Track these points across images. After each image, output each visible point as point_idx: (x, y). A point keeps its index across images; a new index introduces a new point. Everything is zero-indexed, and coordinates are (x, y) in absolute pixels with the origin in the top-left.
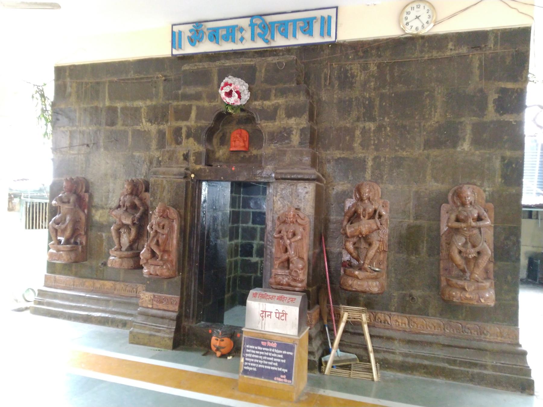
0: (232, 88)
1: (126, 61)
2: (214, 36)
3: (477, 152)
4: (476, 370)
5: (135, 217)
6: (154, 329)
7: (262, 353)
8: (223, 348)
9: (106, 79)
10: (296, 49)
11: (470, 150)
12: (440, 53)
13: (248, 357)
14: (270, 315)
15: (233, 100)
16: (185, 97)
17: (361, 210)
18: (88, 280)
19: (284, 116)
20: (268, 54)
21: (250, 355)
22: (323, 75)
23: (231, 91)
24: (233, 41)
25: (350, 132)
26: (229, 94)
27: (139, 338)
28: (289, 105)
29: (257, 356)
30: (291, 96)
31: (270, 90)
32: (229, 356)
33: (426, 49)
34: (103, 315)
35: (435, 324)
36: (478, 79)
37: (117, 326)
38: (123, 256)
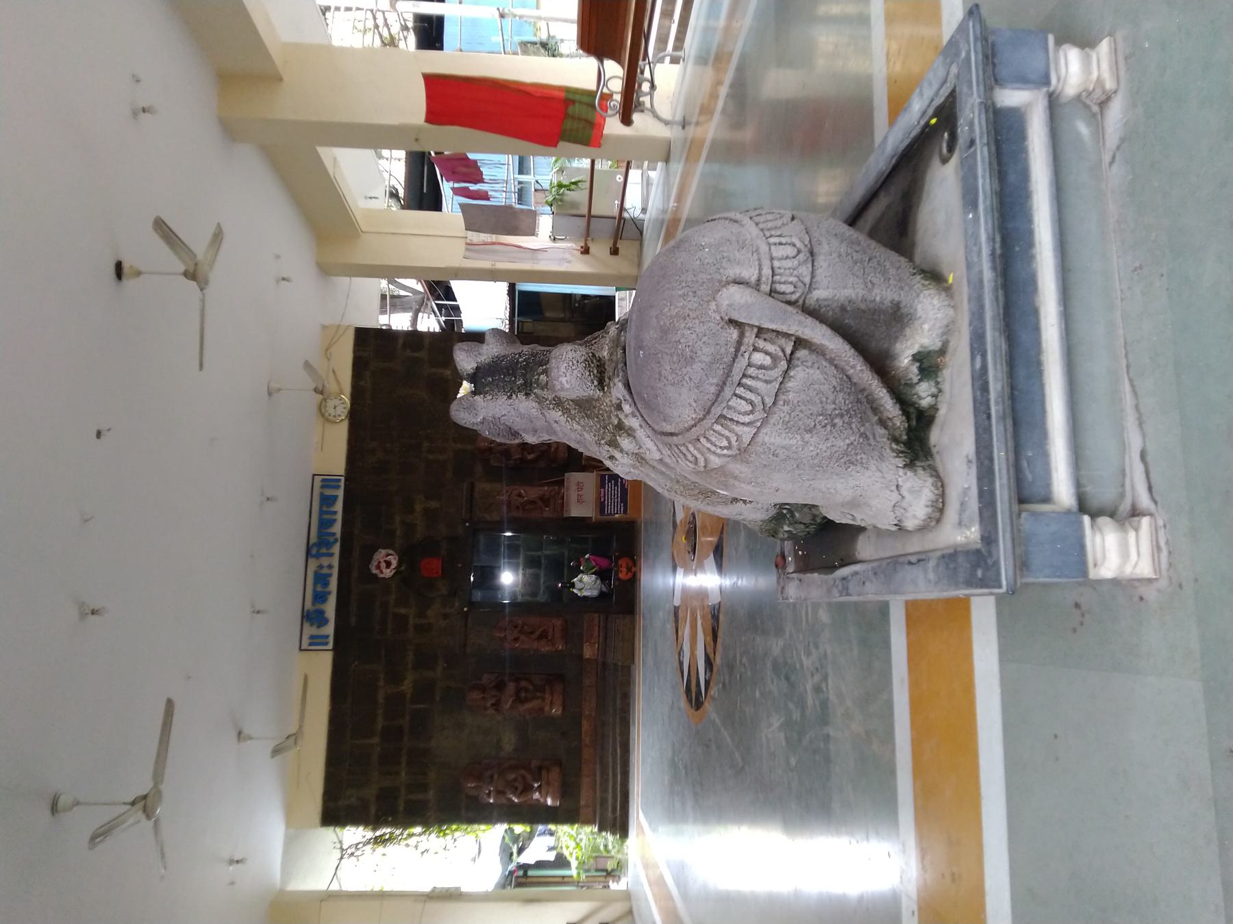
2: (320, 597)
15: (394, 563)
24: (330, 575)
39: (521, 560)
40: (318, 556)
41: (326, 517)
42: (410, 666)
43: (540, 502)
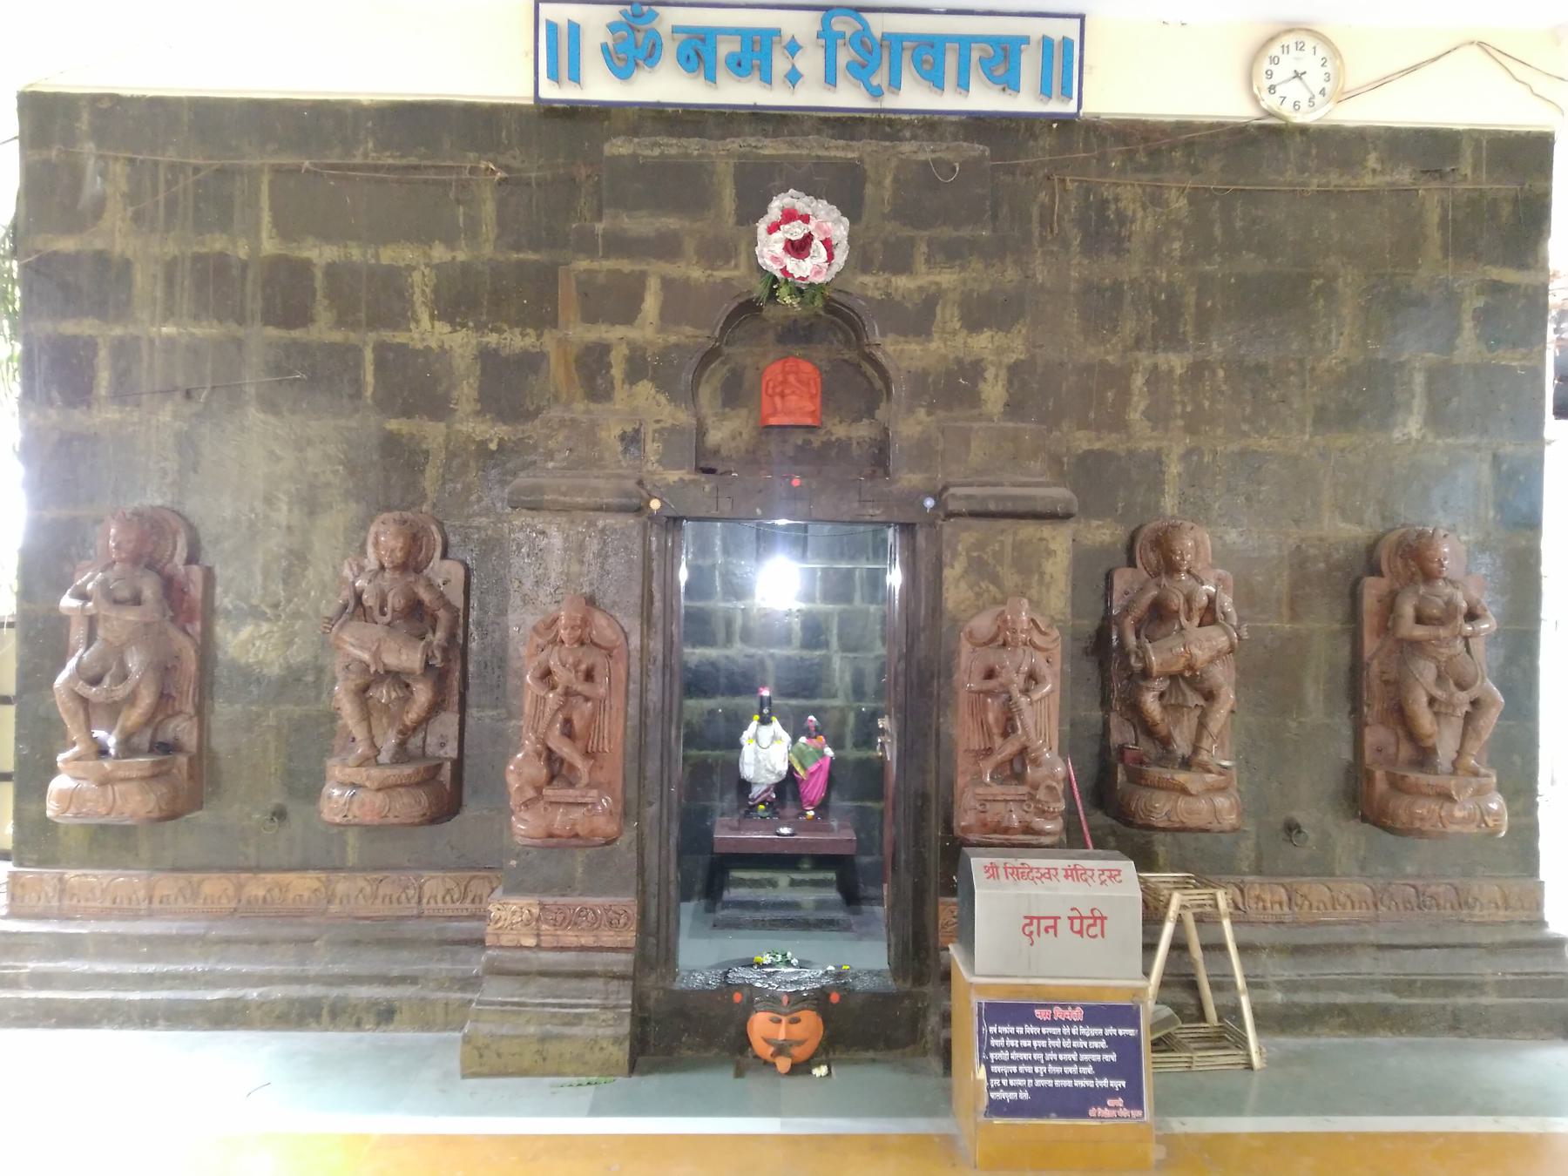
0: (811, 227)
1: (344, 103)
3: (1439, 442)
4: (1462, 1000)
5: (429, 644)
6: (554, 1015)
7: (1043, 1043)
8: (800, 1043)
9: (260, 159)
10: (953, 123)
11: (1424, 437)
12: (1347, 178)
13: (998, 1062)
14: (1055, 927)
15: (802, 269)
16: (619, 245)
17: (1178, 602)
18: (215, 876)
19: (958, 326)
20: (866, 129)
21: (1003, 1055)
22: (1035, 211)
23: (808, 238)
24: (767, 80)
25: (1118, 378)
26: (799, 248)
27: (499, 1055)
28: (972, 291)
29: (1025, 1056)
30: (977, 265)
31: (911, 241)
32: (818, 1065)
33: (1312, 164)
34: (295, 991)
35: (1355, 897)
36: (1439, 256)
37: (358, 1025)
38: (391, 781)
39: (820, 606)
40: (828, 39)
41: (951, 62)
42: (492, 339)
43: (1011, 748)
